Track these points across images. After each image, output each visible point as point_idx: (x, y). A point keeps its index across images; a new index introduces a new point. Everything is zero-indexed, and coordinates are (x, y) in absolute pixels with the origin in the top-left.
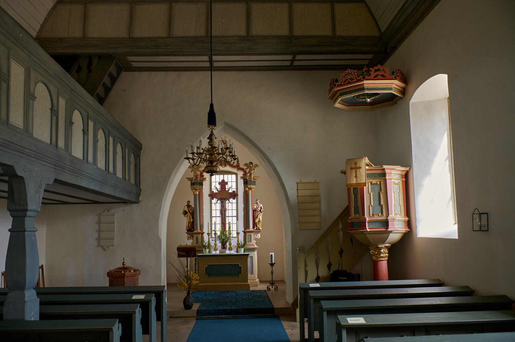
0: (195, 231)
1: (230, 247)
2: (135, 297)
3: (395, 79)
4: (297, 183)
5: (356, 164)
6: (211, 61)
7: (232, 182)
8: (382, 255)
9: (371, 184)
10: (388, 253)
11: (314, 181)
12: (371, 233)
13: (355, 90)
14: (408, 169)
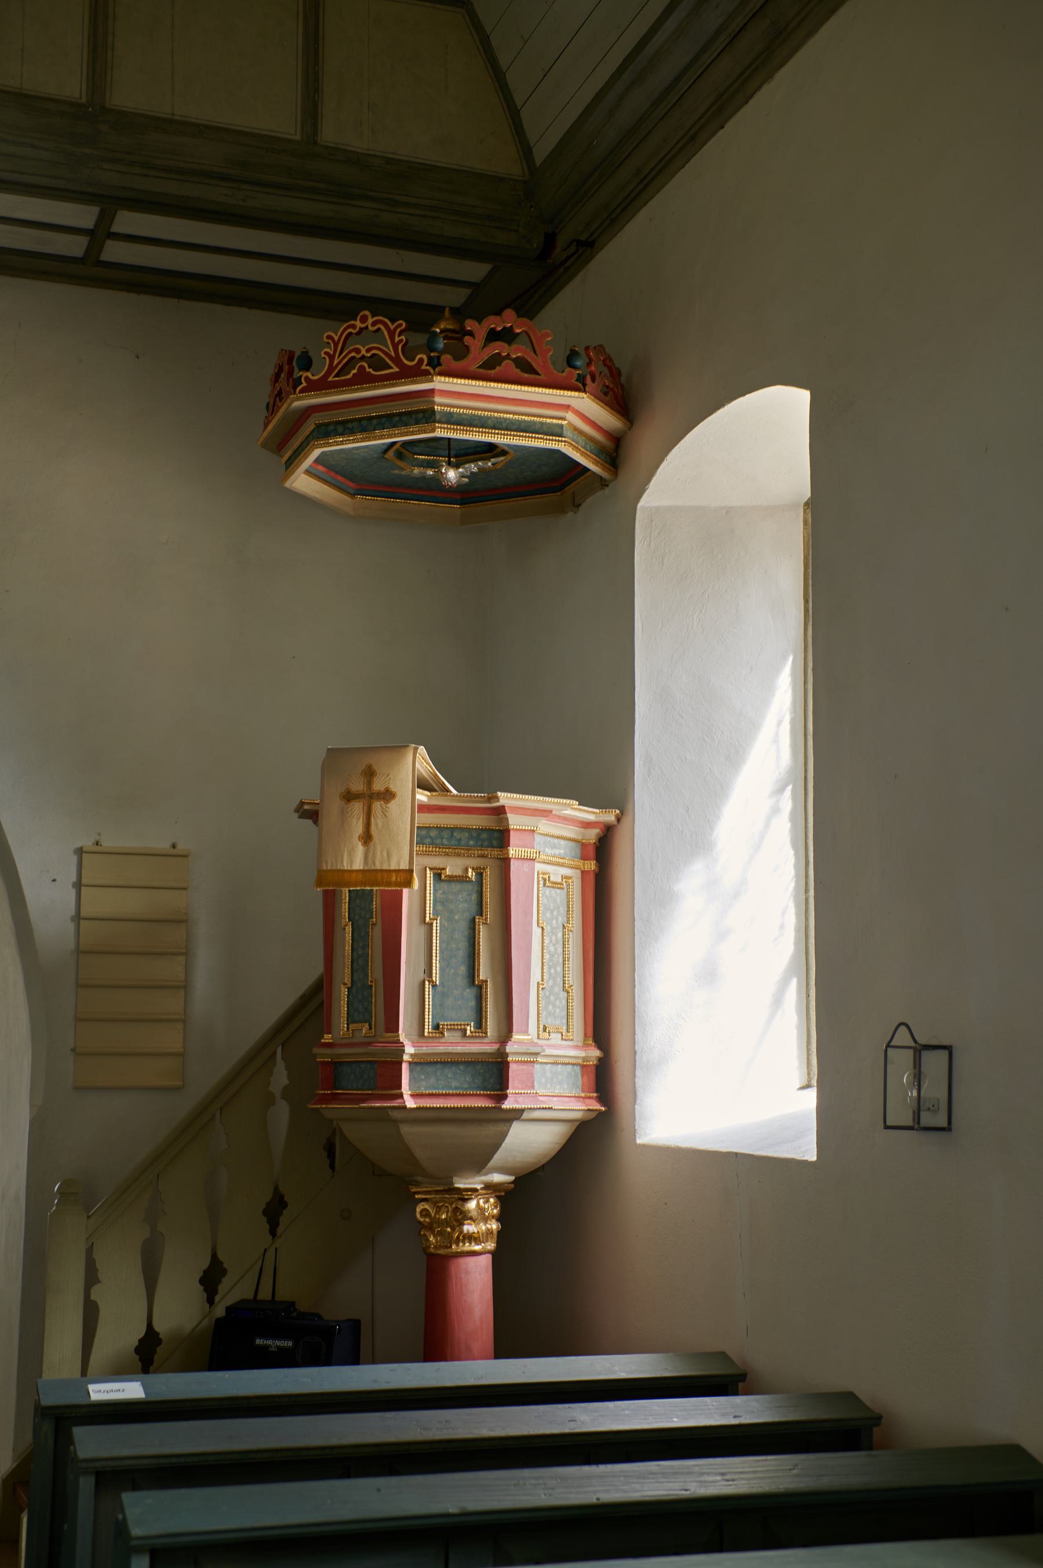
3: (579, 385)
4: (80, 852)
5: (370, 774)
8: (469, 1228)
9: (438, 875)
11: (164, 845)
12: (421, 1116)
14: (610, 817)
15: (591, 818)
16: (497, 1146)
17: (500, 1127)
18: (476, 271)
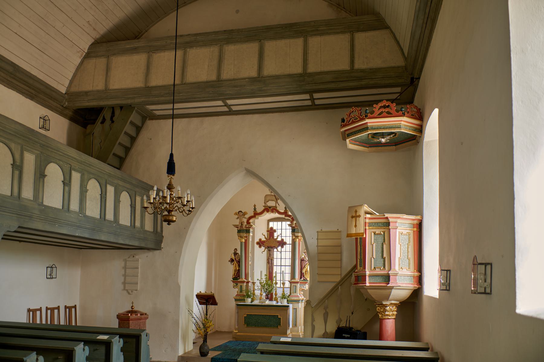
0: (240, 280)
1: (276, 297)
2: (101, 337)
3: (403, 115)
4: (318, 232)
5: (356, 212)
6: (312, 99)
7: (283, 230)
8: (387, 313)
9: (375, 234)
10: (396, 311)
11: (336, 230)
12: (371, 288)
13: (363, 129)
14: (419, 217)
15: (414, 218)
16: (390, 295)
17: (390, 290)
18: (398, 89)
